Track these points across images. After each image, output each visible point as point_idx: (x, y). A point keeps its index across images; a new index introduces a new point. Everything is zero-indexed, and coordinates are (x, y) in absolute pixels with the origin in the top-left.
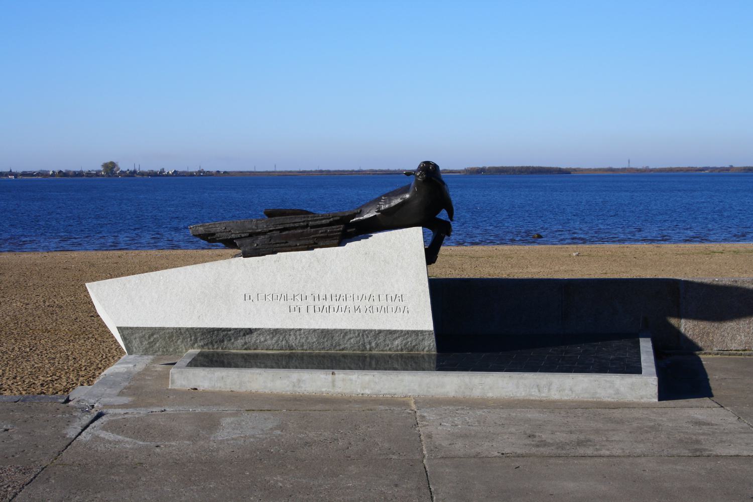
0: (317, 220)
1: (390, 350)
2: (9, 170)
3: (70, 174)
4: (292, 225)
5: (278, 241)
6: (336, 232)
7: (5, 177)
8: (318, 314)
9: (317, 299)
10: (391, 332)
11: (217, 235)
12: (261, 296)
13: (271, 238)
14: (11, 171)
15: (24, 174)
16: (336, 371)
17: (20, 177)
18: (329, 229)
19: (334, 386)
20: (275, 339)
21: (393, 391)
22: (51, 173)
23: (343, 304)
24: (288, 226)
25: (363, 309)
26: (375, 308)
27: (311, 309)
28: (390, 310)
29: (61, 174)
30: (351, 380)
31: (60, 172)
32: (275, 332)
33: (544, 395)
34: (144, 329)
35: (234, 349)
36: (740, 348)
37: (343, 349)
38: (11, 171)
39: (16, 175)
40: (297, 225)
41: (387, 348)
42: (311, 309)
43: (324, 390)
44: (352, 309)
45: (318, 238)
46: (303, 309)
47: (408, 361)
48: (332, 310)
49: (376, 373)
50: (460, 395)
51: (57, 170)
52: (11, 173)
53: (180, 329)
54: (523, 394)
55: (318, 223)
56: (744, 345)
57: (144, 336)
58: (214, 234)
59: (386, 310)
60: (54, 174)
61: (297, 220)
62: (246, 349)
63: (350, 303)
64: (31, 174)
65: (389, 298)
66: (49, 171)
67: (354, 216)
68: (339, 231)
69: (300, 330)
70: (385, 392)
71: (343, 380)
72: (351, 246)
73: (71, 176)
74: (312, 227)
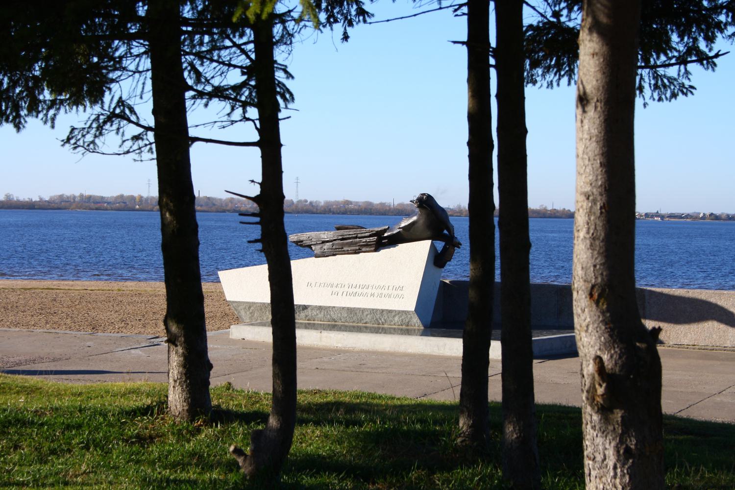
0: (362, 233)
1: (394, 324)
2: (656, 211)
3: (723, 217)
4: (348, 236)
5: (337, 247)
6: (372, 242)
7: (651, 219)
8: (348, 296)
9: (350, 287)
10: (390, 311)
11: (304, 242)
12: (318, 284)
13: (333, 245)
14: (657, 212)
15: (671, 216)
16: (323, 331)
17: (667, 219)
18: (368, 239)
19: (321, 341)
20: (322, 313)
21: (354, 346)
22: (701, 215)
23: (365, 291)
24: (345, 237)
25: (376, 295)
26: (384, 294)
27: (345, 294)
28: (392, 296)
29: (713, 217)
30: (331, 337)
31: (728, 215)
32: (320, 308)
33: (441, 352)
34: (244, 303)
35: (301, 319)
36: (691, 344)
37: (366, 323)
38: (657, 212)
39: (662, 217)
40: (350, 236)
41: (393, 323)
42: (345, 294)
43: (315, 343)
44: (369, 295)
45: (362, 245)
46: (340, 294)
47: (407, 331)
48: (357, 294)
49: (345, 333)
50: (392, 350)
51: (708, 213)
52: (657, 215)
53: (264, 303)
54: (429, 351)
55: (363, 235)
56: (693, 342)
57: (245, 308)
58: (302, 241)
59: (390, 296)
60: (704, 217)
61: (351, 233)
62: (308, 320)
63: (370, 291)
64: (680, 217)
65: (394, 288)
66: (699, 214)
67: (385, 231)
68: (374, 241)
69: (334, 307)
70: (350, 346)
71: (326, 337)
72: (384, 252)
73: (724, 220)
74: (360, 238)
